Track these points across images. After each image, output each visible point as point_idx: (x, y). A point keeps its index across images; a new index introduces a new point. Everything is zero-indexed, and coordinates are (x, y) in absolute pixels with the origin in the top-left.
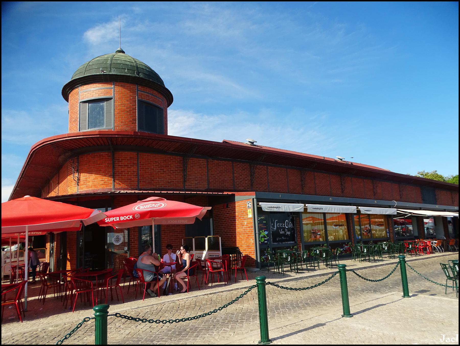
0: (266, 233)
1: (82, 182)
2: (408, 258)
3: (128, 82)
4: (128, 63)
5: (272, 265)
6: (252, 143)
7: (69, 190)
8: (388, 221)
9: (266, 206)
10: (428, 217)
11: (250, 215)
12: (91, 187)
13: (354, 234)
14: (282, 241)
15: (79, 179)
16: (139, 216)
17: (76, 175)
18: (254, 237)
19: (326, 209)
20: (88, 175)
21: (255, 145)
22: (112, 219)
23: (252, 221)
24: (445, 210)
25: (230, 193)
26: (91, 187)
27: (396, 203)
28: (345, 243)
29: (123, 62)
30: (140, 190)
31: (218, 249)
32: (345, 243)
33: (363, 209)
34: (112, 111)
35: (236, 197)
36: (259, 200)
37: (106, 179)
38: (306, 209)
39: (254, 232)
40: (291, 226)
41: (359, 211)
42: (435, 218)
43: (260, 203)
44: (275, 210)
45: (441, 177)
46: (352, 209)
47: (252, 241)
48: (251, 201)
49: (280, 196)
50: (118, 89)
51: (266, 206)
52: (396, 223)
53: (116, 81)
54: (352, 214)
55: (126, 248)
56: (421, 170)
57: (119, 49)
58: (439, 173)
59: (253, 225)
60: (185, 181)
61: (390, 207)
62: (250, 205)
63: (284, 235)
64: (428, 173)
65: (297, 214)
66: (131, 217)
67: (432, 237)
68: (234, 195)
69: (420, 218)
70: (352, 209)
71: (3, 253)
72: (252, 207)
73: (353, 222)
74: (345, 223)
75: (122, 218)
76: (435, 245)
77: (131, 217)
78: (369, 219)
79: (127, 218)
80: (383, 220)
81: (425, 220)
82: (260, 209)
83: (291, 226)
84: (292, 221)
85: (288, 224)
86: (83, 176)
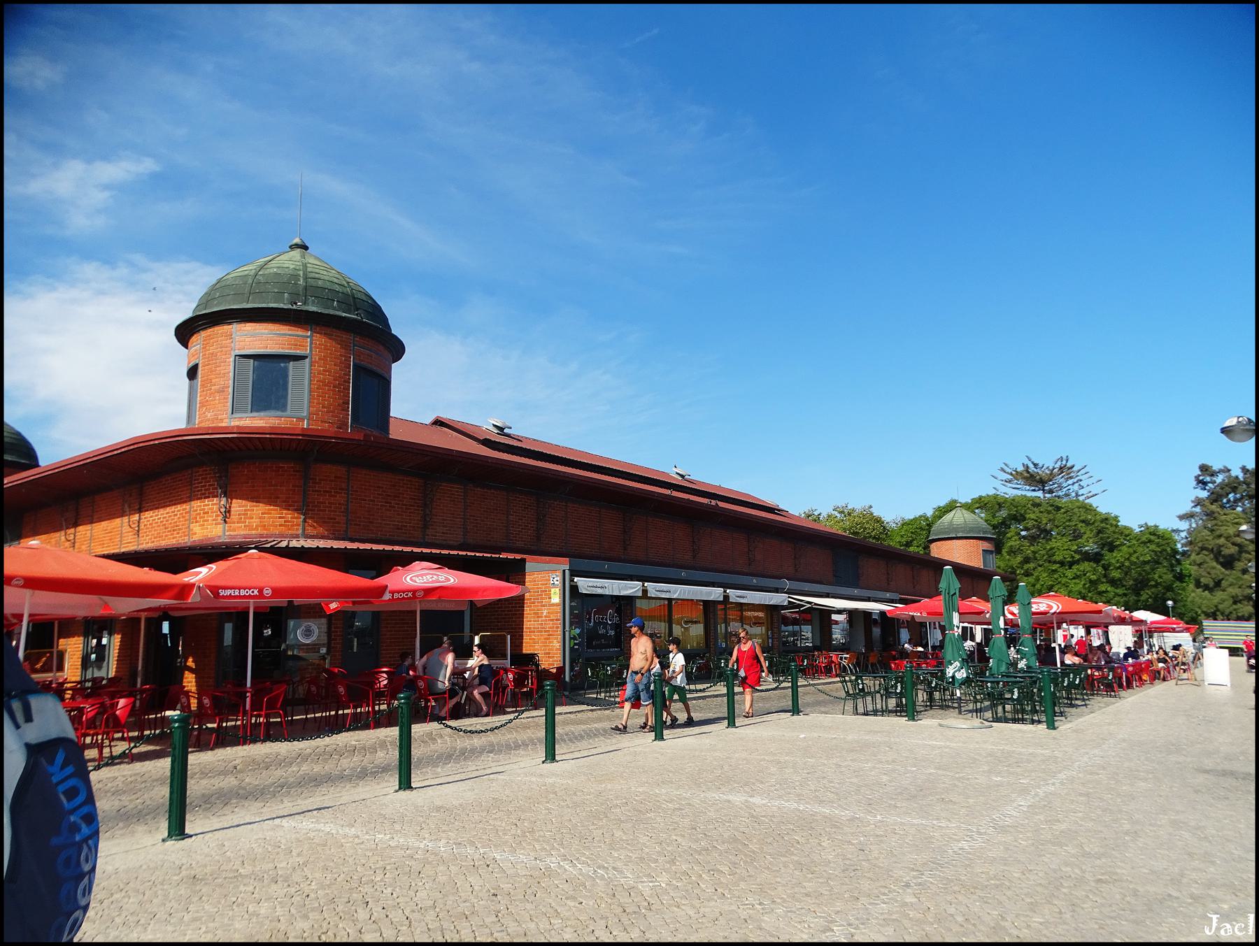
0: (578, 631)
1: (234, 517)
2: (801, 682)
3: (338, 328)
4: (338, 288)
5: (592, 686)
6: (501, 429)
7: (196, 528)
8: (772, 617)
9: (586, 585)
10: (839, 612)
11: (556, 598)
12: (256, 529)
13: (716, 638)
14: (601, 647)
15: (228, 511)
16: (422, 593)
17: (224, 501)
18: (560, 638)
19: (626, 588)
20: (249, 504)
21: (508, 436)
22: (228, 592)
23: (560, 609)
24: (868, 600)
25: (518, 557)
26: (256, 529)
27: (788, 584)
28: (698, 655)
29: (328, 285)
30: (352, 541)
31: (504, 656)
32: (698, 655)
33: (733, 594)
34: (306, 382)
35: (529, 566)
36: (574, 573)
37: (288, 515)
38: (645, 591)
39: (561, 629)
40: (616, 620)
41: (726, 597)
42: (852, 613)
43: (576, 579)
44: (599, 591)
45: (878, 520)
46: (715, 593)
47: (557, 644)
48: (560, 574)
49: (606, 566)
50: (320, 339)
51: (586, 585)
52: (786, 621)
53: (317, 324)
54: (714, 602)
55: (323, 651)
56: (841, 504)
57: (297, 241)
58: (876, 512)
59: (560, 616)
60: (425, 527)
61: (777, 590)
62: (557, 579)
63: (605, 636)
64: (853, 510)
65: (630, 599)
66: (410, 594)
67: (843, 648)
68: (524, 561)
69: (826, 613)
70: (715, 593)
71: (1250, 579)
72: (561, 585)
73: (715, 615)
74: (701, 618)
75: (243, 593)
76: (844, 662)
77: (410, 594)
78: (741, 611)
79: (250, 592)
80: (761, 614)
81: (834, 617)
82: (574, 588)
83: (616, 620)
84: (619, 611)
85: (610, 617)
86: (238, 506)
